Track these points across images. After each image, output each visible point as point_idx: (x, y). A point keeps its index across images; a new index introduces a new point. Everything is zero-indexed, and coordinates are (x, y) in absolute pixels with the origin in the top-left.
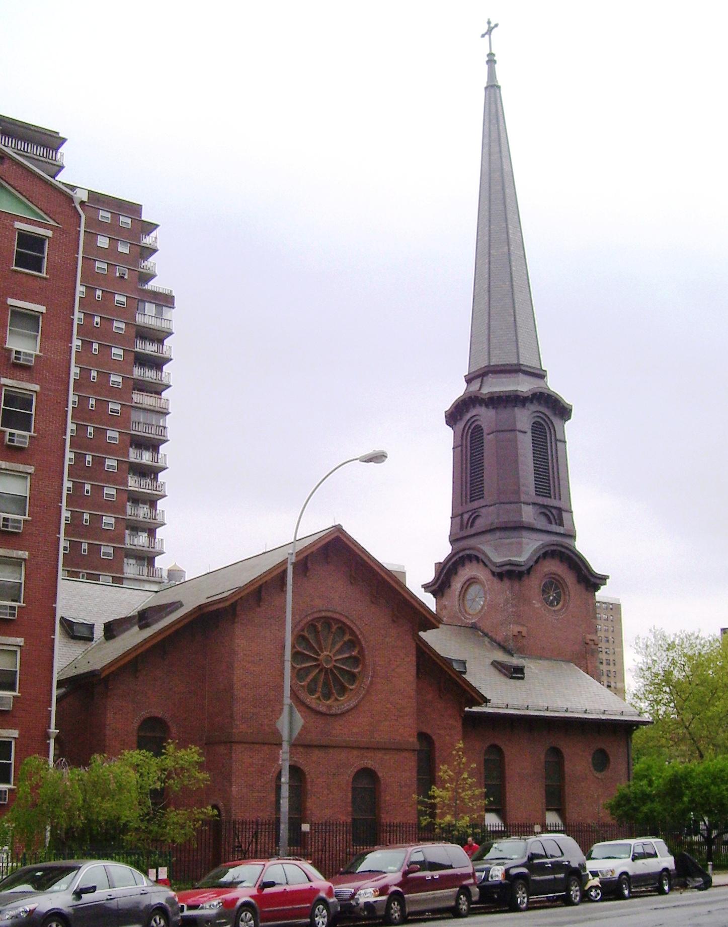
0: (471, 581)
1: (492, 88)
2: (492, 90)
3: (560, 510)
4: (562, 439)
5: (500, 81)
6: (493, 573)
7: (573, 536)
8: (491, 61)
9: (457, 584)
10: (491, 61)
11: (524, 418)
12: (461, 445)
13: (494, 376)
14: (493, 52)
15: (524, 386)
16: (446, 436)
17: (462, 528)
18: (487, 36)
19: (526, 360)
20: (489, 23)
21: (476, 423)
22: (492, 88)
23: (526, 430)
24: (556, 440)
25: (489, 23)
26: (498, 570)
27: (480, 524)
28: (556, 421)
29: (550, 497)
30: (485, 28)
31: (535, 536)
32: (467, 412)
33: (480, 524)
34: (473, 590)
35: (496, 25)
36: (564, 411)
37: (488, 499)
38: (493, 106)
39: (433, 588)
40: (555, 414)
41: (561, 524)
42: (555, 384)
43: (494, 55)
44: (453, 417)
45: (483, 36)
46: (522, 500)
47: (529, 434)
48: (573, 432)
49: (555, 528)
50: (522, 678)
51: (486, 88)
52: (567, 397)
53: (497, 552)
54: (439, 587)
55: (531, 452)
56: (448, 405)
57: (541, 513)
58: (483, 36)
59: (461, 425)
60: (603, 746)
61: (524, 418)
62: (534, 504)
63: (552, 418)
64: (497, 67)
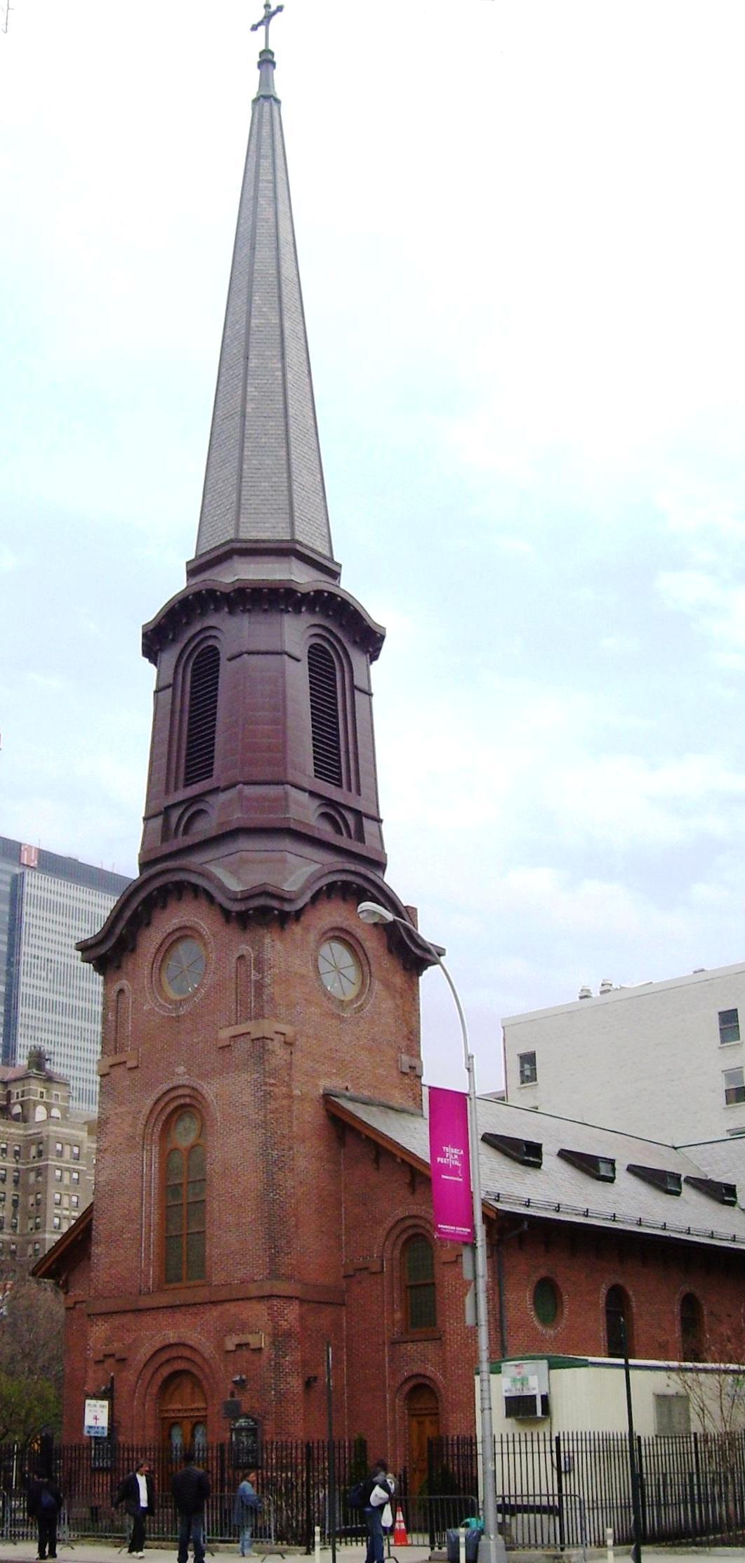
0: (184, 934)
1: (266, 100)
2: (266, 104)
3: (358, 814)
4: (372, 812)
5: (280, 90)
6: (227, 915)
7: (381, 865)
8: (266, 60)
9: (151, 940)
10: (266, 60)
11: (295, 633)
12: (173, 686)
13: (243, 559)
14: (271, 47)
15: (303, 578)
16: (147, 675)
17: (166, 834)
18: (262, 29)
19: (307, 537)
20: (267, 6)
21: (211, 642)
22: (266, 100)
23: (296, 653)
24: (354, 688)
25: (267, 6)
26: (236, 907)
27: (205, 827)
28: (357, 658)
29: (340, 786)
30: (261, 14)
31: (308, 851)
32: (188, 623)
33: (205, 827)
34: (184, 951)
35: (280, 9)
37: (220, 775)
38: (265, 163)
39: (102, 950)
40: (355, 643)
41: (361, 839)
42: (354, 585)
43: (272, 54)
44: (156, 640)
45: (254, 28)
46: (290, 778)
47: (305, 660)
48: (384, 676)
49: (343, 841)
50: (545, 1399)
51: (255, 101)
52: (376, 610)
53: (232, 874)
54: (114, 948)
55: (309, 723)
56: (151, 610)
57: (325, 815)
58: (254, 28)
59: (169, 657)
60: (698, 1293)
61: (295, 633)
62: (313, 794)
63: (347, 646)
64: (278, 75)
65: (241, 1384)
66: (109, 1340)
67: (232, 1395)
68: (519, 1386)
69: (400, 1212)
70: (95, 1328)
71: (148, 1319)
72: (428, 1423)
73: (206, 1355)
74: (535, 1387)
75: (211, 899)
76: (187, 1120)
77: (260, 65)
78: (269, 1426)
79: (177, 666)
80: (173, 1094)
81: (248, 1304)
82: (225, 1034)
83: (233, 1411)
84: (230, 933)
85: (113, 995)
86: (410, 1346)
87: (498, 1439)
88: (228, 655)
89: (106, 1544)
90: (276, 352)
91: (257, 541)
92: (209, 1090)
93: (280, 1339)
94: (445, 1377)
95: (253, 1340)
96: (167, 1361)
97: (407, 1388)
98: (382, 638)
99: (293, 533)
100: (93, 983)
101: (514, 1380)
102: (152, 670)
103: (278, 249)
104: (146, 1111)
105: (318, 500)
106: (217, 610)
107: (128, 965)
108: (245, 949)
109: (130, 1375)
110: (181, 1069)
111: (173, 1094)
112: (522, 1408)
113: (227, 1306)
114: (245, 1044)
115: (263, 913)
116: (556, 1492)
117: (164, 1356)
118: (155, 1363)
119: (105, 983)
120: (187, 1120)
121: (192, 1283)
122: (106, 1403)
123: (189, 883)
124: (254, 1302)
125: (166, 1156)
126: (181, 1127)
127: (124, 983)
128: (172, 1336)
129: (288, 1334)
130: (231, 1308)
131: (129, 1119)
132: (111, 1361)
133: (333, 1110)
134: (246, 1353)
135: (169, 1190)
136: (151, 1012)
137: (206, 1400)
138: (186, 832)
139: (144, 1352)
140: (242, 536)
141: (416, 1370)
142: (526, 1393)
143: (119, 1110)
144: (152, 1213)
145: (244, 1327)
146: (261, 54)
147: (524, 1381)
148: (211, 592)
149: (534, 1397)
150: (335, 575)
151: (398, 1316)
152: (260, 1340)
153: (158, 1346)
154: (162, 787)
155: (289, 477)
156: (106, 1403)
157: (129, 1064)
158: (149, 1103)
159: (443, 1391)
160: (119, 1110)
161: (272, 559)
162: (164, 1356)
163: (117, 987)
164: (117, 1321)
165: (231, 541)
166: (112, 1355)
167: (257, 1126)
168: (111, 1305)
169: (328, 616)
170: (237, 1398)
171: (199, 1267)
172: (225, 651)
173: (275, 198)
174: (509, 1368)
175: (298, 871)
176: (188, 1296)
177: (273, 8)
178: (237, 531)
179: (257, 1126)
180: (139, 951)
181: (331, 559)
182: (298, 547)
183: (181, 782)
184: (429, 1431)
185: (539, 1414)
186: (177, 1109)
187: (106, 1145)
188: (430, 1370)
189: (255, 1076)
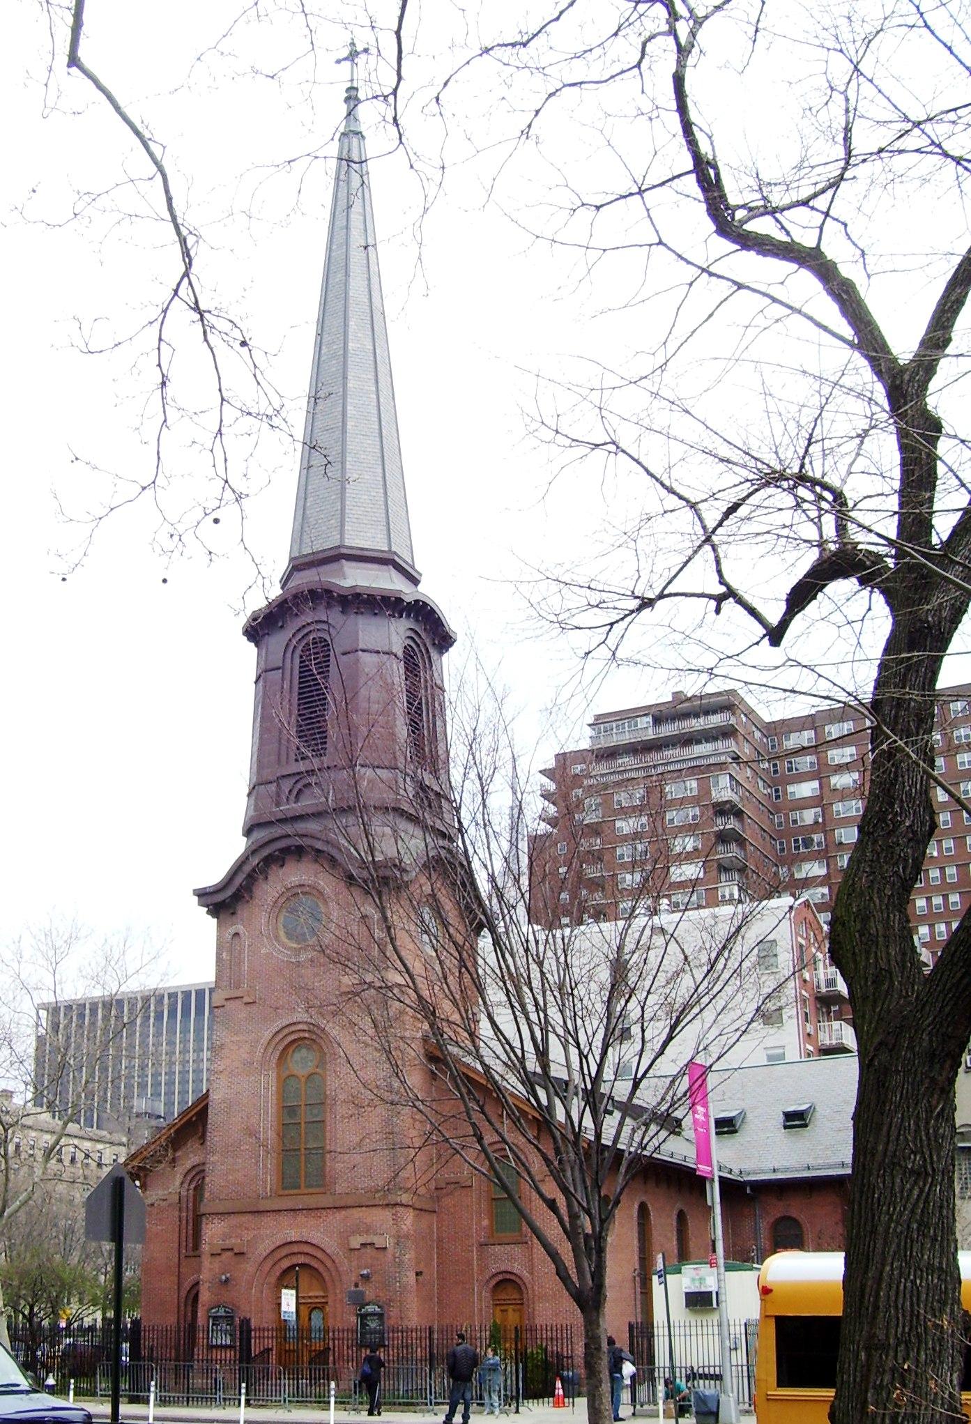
36: (444, 640)
39: (220, 898)
52: (453, 621)
59: (278, 641)
63: (431, 650)
65: (366, 1278)
66: (225, 1237)
67: (356, 1285)
68: (697, 1284)
70: (210, 1226)
71: (268, 1220)
72: (510, 1313)
74: (710, 1284)
75: (333, 861)
76: (304, 1051)
77: (347, 100)
78: (394, 1312)
80: (293, 1028)
81: (374, 1210)
83: (358, 1301)
86: (497, 1248)
87: (732, 1323)
88: (342, 650)
89: (313, 1408)
90: (371, 376)
91: (362, 549)
93: (399, 1239)
94: (532, 1274)
95: (379, 1242)
96: (286, 1256)
97: (493, 1282)
98: (451, 645)
99: (390, 545)
101: (693, 1280)
102: (251, 649)
103: (369, 279)
104: (264, 1041)
105: (404, 515)
106: (329, 606)
107: (243, 911)
109: (249, 1267)
111: (293, 1028)
112: (700, 1301)
113: (355, 1211)
115: (381, 882)
116: (667, 1364)
117: (284, 1251)
118: (278, 1255)
120: (304, 1051)
121: (311, 1190)
122: (294, 1292)
123: (312, 847)
124: (380, 1209)
125: (285, 1082)
126: (297, 1056)
127: (239, 928)
128: (293, 1235)
129: (407, 1237)
130: (356, 1213)
131: (247, 1047)
132: (229, 1254)
134: (369, 1250)
135: (288, 1111)
136: (269, 955)
137: (325, 1289)
139: (264, 1248)
140: (347, 543)
142: (703, 1290)
143: (235, 1038)
144: (268, 1129)
145: (368, 1230)
146: (348, 90)
147: (702, 1280)
148: (328, 592)
149: (711, 1293)
150: (415, 582)
151: (485, 1222)
152: (388, 1242)
153: (278, 1244)
154: (273, 758)
155: (386, 493)
156: (294, 1292)
157: (246, 999)
158: (268, 1035)
159: (529, 1286)
161: (375, 566)
162: (284, 1251)
163: (232, 930)
164: (234, 1220)
165: (339, 547)
168: (228, 1206)
169: (417, 621)
170: (360, 1288)
171: (321, 1180)
172: (338, 646)
173: (366, 231)
174: (688, 1269)
175: (411, 846)
176: (312, 1201)
177: (360, 48)
178: (342, 534)
181: (413, 567)
182: (397, 559)
184: (512, 1318)
185: (715, 1305)
188: (516, 1268)
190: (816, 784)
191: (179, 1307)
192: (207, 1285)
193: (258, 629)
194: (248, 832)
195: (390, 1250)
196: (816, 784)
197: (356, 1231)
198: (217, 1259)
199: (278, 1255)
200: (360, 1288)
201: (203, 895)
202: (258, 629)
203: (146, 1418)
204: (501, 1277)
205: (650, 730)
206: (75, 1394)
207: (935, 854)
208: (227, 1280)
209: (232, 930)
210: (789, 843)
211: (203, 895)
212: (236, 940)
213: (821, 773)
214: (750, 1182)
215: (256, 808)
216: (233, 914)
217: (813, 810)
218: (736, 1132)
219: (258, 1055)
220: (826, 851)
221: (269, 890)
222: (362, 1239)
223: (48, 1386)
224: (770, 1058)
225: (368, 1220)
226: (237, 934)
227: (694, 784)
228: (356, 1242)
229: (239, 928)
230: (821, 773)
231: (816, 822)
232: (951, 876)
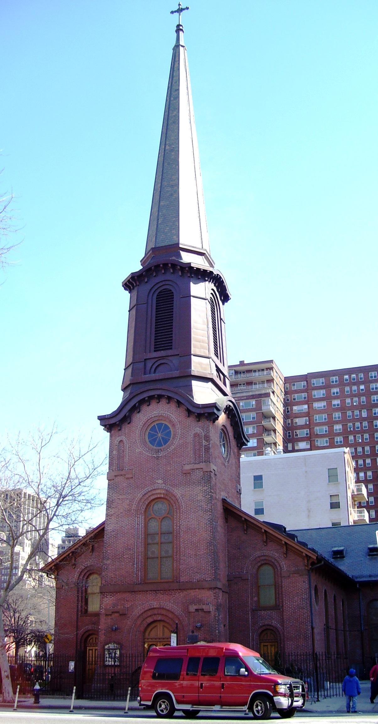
16: (126, 296)
36: (225, 298)
39: (112, 421)
65: (198, 628)
67: (193, 632)
69: (258, 553)
73: (176, 613)
77: (176, 31)
79: (148, 295)
82: (187, 467)
84: (191, 421)
85: (116, 442)
86: (263, 612)
87: (318, 654)
92: (178, 492)
97: (260, 630)
98: (229, 300)
100: (103, 437)
102: (127, 294)
107: (126, 428)
108: (198, 430)
110: (160, 481)
111: (154, 492)
113: (189, 591)
114: (199, 474)
117: (149, 613)
119: (111, 436)
127: (123, 438)
128: (155, 604)
129: (221, 605)
130: (192, 593)
132: (116, 615)
133: (227, 506)
136: (140, 453)
138: (155, 372)
139: (137, 611)
141: (266, 623)
143: (120, 497)
145: (200, 601)
152: (211, 608)
156: (175, 635)
158: (139, 495)
160: (120, 497)
163: (119, 439)
164: (119, 596)
166: (118, 612)
167: (206, 511)
169: (215, 285)
170: (195, 634)
179: (206, 511)
180: (133, 424)
183: (153, 349)
186: (154, 499)
187: (112, 513)
188: (274, 623)
189: (205, 488)
190: (306, 406)
191: (77, 644)
192: (103, 632)
193: (131, 284)
194: (124, 389)
195: (212, 614)
196: (306, 406)
197: (193, 602)
198: (110, 617)
199: (145, 615)
200: (195, 634)
201: (102, 419)
202: (131, 284)
203: (124, 709)
204: (264, 628)
205: (233, 376)
206: (130, 701)
207: (360, 441)
208: (116, 629)
209: (119, 439)
210: (293, 433)
211: (102, 419)
212: (121, 444)
213: (309, 401)
214: (358, 582)
215: (133, 374)
216: (120, 430)
217: (304, 418)
218: (344, 557)
219: (134, 507)
220: (310, 437)
221: (141, 418)
222: (196, 607)
223: (34, 690)
224: (333, 524)
225: (200, 596)
226: (121, 441)
227: (254, 403)
228: (192, 608)
229: (123, 438)
230: (309, 401)
231: (306, 424)
232: (367, 451)
